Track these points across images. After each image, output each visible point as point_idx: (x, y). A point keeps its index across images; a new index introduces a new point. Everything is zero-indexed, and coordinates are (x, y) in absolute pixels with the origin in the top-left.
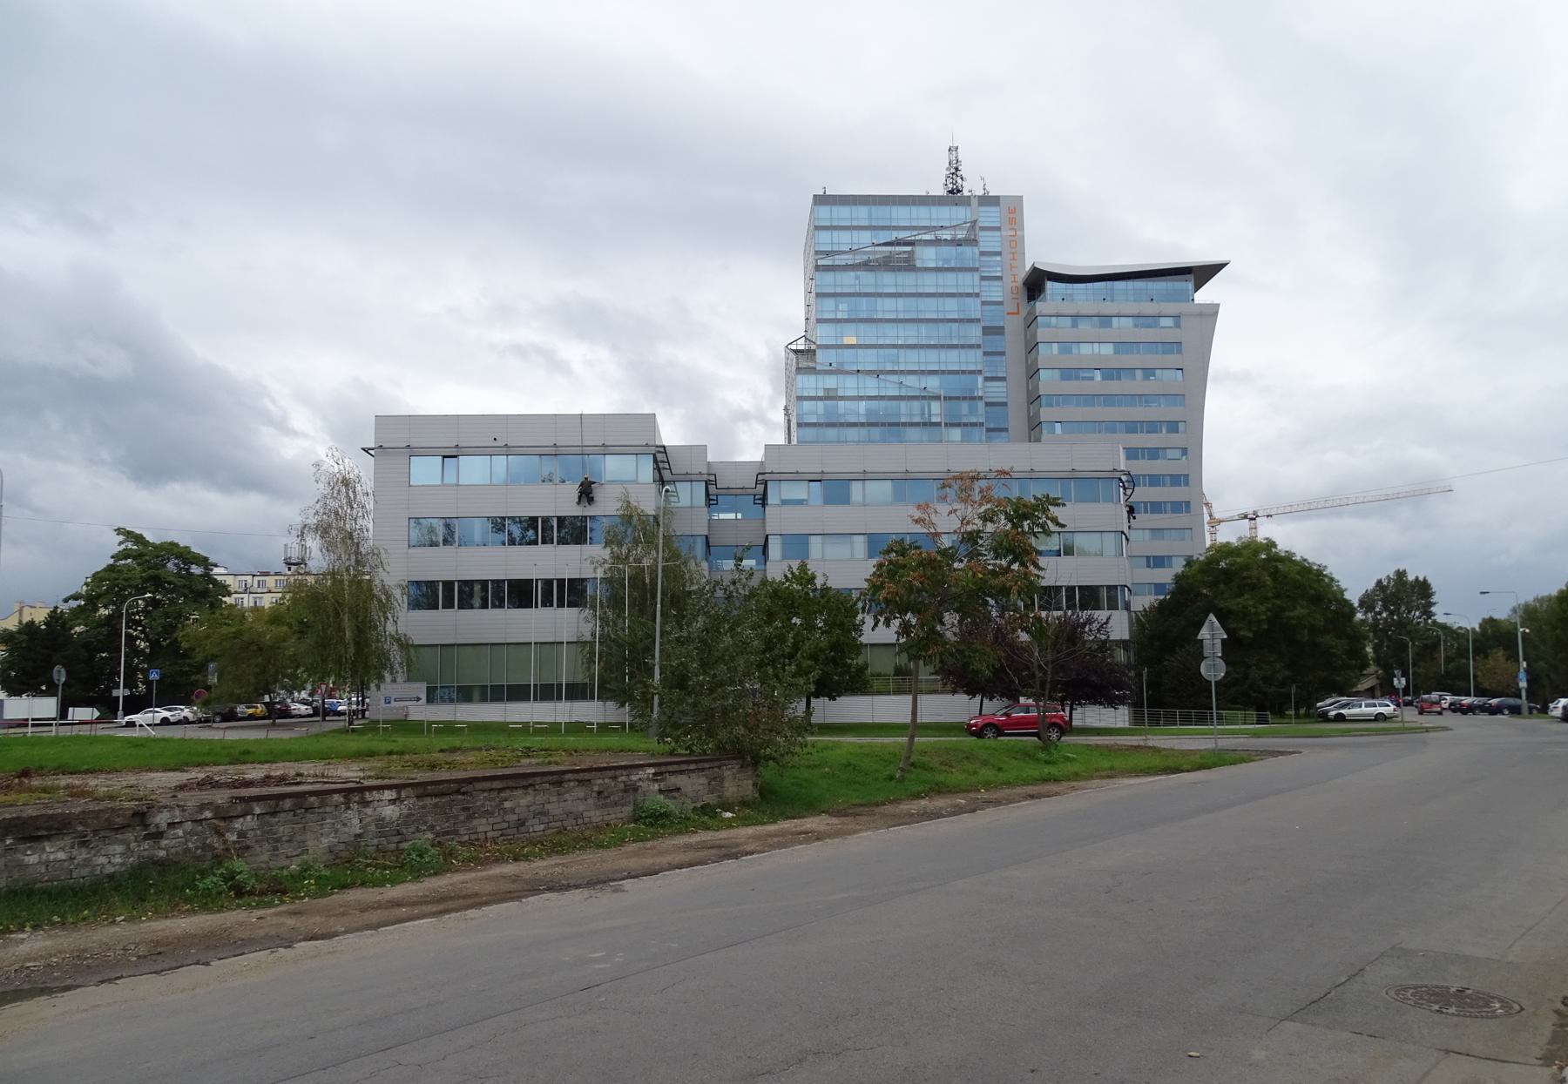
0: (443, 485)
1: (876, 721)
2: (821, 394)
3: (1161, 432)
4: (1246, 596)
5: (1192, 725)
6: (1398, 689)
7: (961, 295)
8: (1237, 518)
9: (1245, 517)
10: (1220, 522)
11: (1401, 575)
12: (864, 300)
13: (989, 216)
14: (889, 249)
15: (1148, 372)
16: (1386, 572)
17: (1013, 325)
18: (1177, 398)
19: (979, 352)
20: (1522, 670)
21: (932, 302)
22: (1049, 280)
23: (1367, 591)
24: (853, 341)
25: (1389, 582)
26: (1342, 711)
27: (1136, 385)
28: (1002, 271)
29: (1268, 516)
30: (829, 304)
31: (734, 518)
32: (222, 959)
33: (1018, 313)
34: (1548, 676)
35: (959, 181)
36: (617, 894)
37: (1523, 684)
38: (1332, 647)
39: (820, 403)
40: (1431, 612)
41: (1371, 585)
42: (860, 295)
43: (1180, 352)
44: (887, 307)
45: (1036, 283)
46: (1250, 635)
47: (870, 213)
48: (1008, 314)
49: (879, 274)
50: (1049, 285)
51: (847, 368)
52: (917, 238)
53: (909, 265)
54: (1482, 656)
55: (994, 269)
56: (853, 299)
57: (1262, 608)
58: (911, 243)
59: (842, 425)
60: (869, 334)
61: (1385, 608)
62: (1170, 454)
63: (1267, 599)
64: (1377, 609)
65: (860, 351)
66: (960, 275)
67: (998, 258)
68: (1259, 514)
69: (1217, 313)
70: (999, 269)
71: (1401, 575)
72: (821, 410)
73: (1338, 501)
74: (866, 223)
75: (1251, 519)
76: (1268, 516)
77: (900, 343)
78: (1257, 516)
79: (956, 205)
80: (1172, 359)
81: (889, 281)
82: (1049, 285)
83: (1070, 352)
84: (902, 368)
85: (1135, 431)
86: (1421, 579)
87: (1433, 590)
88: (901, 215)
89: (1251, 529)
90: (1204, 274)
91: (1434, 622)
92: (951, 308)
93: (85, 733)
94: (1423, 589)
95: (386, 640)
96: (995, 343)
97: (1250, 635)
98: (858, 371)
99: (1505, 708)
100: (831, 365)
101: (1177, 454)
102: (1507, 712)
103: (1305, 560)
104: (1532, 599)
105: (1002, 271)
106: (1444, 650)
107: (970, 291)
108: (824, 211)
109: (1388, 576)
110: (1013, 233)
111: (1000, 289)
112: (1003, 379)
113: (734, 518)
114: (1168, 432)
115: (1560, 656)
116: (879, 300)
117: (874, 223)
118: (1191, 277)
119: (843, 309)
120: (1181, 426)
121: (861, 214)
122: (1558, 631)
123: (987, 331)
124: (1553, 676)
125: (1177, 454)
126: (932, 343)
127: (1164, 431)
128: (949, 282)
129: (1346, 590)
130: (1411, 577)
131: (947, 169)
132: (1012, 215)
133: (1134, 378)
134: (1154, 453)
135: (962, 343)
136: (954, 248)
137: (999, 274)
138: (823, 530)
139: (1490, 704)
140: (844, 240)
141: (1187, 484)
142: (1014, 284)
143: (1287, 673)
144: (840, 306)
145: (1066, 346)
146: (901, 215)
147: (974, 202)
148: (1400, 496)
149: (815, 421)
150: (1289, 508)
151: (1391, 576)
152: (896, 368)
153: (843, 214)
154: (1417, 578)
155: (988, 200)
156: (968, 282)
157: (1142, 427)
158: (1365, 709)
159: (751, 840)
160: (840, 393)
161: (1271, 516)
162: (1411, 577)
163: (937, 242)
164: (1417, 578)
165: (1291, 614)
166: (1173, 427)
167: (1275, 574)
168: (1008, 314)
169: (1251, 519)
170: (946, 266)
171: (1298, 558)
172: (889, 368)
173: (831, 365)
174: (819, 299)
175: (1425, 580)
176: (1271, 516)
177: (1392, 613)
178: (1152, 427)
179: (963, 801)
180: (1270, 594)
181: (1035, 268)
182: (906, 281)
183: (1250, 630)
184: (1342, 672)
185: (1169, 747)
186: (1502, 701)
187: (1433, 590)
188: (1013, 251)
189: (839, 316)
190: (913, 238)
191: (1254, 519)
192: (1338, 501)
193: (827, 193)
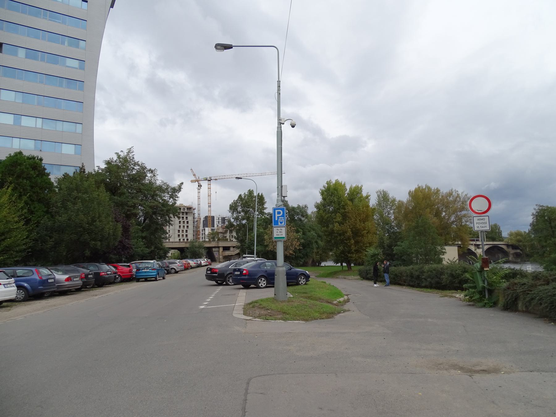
9: (206, 180)
10: (212, 180)
23: (234, 201)
25: (245, 197)
29: (215, 180)
32: (230, 237)
34: (316, 242)
36: (193, 231)
41: (236, 198)
62: (69, 62)
68: (212, 178)
71: (251, 192)
73: (249, 175)
75: (209, 180)
76: (215, 180)
85: (35, 58)
87: (266, 201)
93: (457, 285)
109: (245, 193)
124: (320, 242)
125: (75, 64)
134: (55, 58)
148: (266, 174)
159: (483, 278)
169: (209, 180)
179: (343, 255)
191: (210, 181)
192: (249, 175)
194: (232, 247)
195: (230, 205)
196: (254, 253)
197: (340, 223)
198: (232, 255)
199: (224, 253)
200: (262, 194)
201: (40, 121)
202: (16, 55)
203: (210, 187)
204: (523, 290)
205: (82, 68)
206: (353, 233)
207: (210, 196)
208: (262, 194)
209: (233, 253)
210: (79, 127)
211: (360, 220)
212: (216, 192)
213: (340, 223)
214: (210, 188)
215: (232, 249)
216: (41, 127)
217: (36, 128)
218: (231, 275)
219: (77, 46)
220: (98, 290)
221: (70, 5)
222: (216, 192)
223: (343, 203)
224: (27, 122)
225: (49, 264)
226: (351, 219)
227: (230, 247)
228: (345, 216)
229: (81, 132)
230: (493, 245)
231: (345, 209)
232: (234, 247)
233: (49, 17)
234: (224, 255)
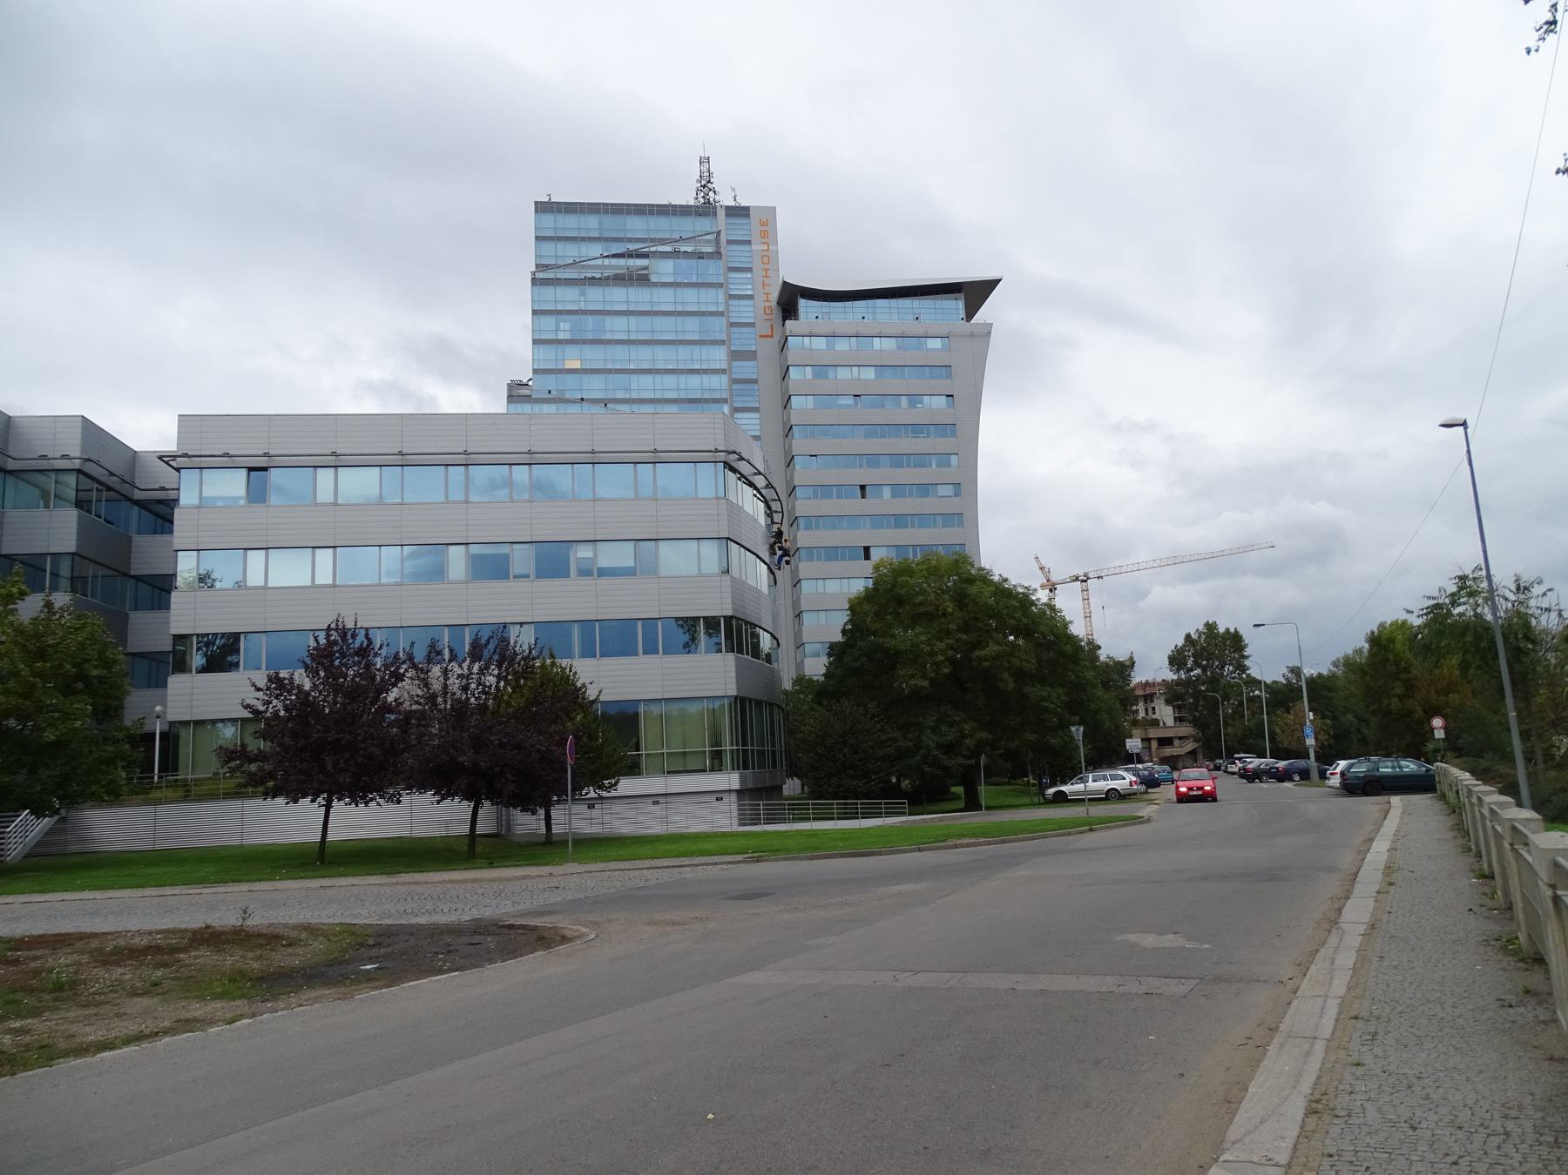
1: (161, 845)
3: (931, 466)
4: (918, 629)
5: (808, 819)
6: (1132, 754)
7: (703, 314)
8: (1069, 580)
9: (1077, 579)
11: (1211, 627)
12: (590, 319)
13: (738, 230)
14: (622, 262)
15: (914, 398)
16: (1194, 626)
17: (768, 348)
18: (946, 429)
19: (725, 379)
20: (1308, 723)
21: (669, 321)
22: (803, 296)
23: (1176, 646)
24: (577, 365)
25: (1200, 637)
26: (1063, 788)
27: (902, 412)
28: (753, 289)
29: (1099, 578)
30: (548, 322)
33: (772, 336)
35: (711, 194)
37: (1310, 741)
38: (1043, 699)
40: (1245, 666)
41: (1180, 642)
42: (584, 312)
43: (949, 376)
44: (618, 327)
45: (790, 300)
46: (925, 683)
47: (600, 223)
48: (761, 336)
49: (607, 289)
50: (802, 303)
51: (568, 396)
52: (653, 249)
53: (642, 279)
54: (1283, 709)
55: (745, 287)
56: (578, 317)
57: (940, 645)
58: (645, 256)
60: (595, 356)
61: (1197, 664)
63: (948, 632)
64: (1189, 666)
65: (585, 377)
66: (703, 291)
67: (749, 275)
69: (989, 333)
70: (750, 287)
71: (1211, 627)
74: (596, 235)
75: (1083, 581)
76: (1099, 578)
77: (632, 367)
78: (1089, 578)
80: (944, 385)
81: (618, 297)
82: (802, 303)
83: (825, 376)
84: (635, 395)
86: (1232, 630)
87: (1246, 642)
88: (636, 226)
89: (1083, 591)
90: (975, 293)
91: (1248, 676)
92: (691, 327)
94: (1235, 641)
95: (888, 747)
96: (745, 369)
97: (925, 683)
98: (582, 399)
99: (1294, 773)
100: (549, 392)
101: (949, 490)
102: (1297, 778)
103: (1006, 580)
104: (1351, 652)
105: (753, 289)
107: (712, 308)
108: (549, 220)
111: (752, 309)
112: (756, 410)
114: (938, 466)
115: (1372, 707)
116: (608, 319)
117: (606, 235)
118: (962, 295)
119: (565, 329)
120: (954, 459)
121: (591, 223)
122: (1368, 678)
123: (736, 356)
125: (949, 490)
126: (671, 367)
128: (691, 299)
129: (1071, 622)
130: (1222, 630)
131: (697, 181)
132: (763, 228)
133: (899, 404)
134: (925, 489)
135: (705, 368)
136: (695, 261)
137: (750, 293)
138: (267, 542)
139: (1277, 768)
140: (570, 252)
142: (767, 304)
143: (984, 735)
144: (562, 324)
145: (821, 369)
146: (636, 226)
147: (721, 213)
148: (1225, 553)
150: (1118, 569)
151: (1200, 629)
152: (628, 396)
153: (570, 223)
154: (1228, 630)
155: (738, 212)
156: (711, 299)
158: (1096, 783)
162: (1222, 630)
163: (675, 254)
164: (1228, 630)
165: (982, 653)
166: (944, 458)
167: (961, 598)
168: (761, 336)
169: (1083, 581)
170: (686, 281)
171: (996, 578)
172: (620, 395)
173: (549, 392)
174: (536, 317)
175: (1236, 632)
176: (1102, 577)
177: (1204, 669)
178: (920, 459)
180: (952, 627)
181: (784, 282)
182: (638, 297)
183: (924, 676)
184: (1060, 733)
186: (1291, 764)
187: (1246, 642)
188: (766, 267)
189: (561, 337)
190: (647, 250)
191: (1086, 581)
193: (552, 200)
194: (1176, 737)
195: (1169, 657)
196: (658, 650)
197: (1400, 698)
198: (1178, 756)
199: (1161, 751)
200: (1236, 629)
203: (1088, 595)
205: (957, 494)
206: (1425, 712)
207: (1090, 617)
208: (1236, 629)
209: (1181, 751)
211: (1436, 691)
212: (1103, 607)
213: (1400, 698)
214: (1088, 599)
215: (1176, 742)
218: (183, 1004)
220: (1071, 808)
221: (933, 407)
222: (1103, 607)
223: (1403, 663)
226: (1420, 690)
227: (1172, 738)
228: (1410, 686)
230: (935, 808)
231: (1409, 673)
232: (1180, 738)
233: (912, 433)
234: (1162, 755)
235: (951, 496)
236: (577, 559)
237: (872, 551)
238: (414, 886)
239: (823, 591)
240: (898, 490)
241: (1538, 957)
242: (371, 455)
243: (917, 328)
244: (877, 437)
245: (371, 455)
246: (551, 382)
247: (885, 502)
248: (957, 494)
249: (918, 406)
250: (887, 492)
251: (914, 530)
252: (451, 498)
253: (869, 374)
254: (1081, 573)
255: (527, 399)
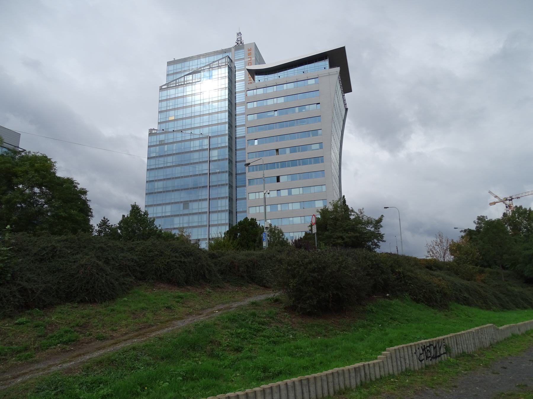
0: (281, 210)
2: (158, 143)
10: (513, 199)
27: (296, 114)
29: (518, 198)
31: (219, 206)
39: (157, 147)
59: (165, 156)
68: (513, 197)
72: (157, 150)
75: (510, 200)
76: (518, 198)
79: (225, 52)
85: (295, 151)
106: (525, 324)
110: (250, 59)
113: (219, 206)
125: (317, 146)
127: (311, 136)
134: (304, 148)
141: (322, 161)
149: (155, 155)
157: (299, 149)
160: (166, 142)
161: (519, 198)
169: (510, 200)
185: (338, 189)
191: (511, 200)
200: (308, 227)
201: (301, 189)
202: (285, 153)
204: (32, 368)
205: (321, 147)
208: (308, 227)
210: (324, 187)
216: (302, 193)
217: (300, 194)
219: (317, 135)
224: (295, 192)
225: (177, 291)
229: (325, 191)
235: (317, 149)
236: (300, 209)
237: (281, 178)
238: (411, 366)
239: (258, 198)
240: (293, 149)
241: (286, 365)
242: (10, 145)
243: (304, 77)
244: (284, 127)
245: (10, 145)
246: (163, 126)
247: (287, 156)
248: (321, 147)
249: (303, 110)
250: (288, 151)
251: (300, 167)
252: (300, 193)
253: (281, 100)
254: (508, 196)
255: (156, 134)
